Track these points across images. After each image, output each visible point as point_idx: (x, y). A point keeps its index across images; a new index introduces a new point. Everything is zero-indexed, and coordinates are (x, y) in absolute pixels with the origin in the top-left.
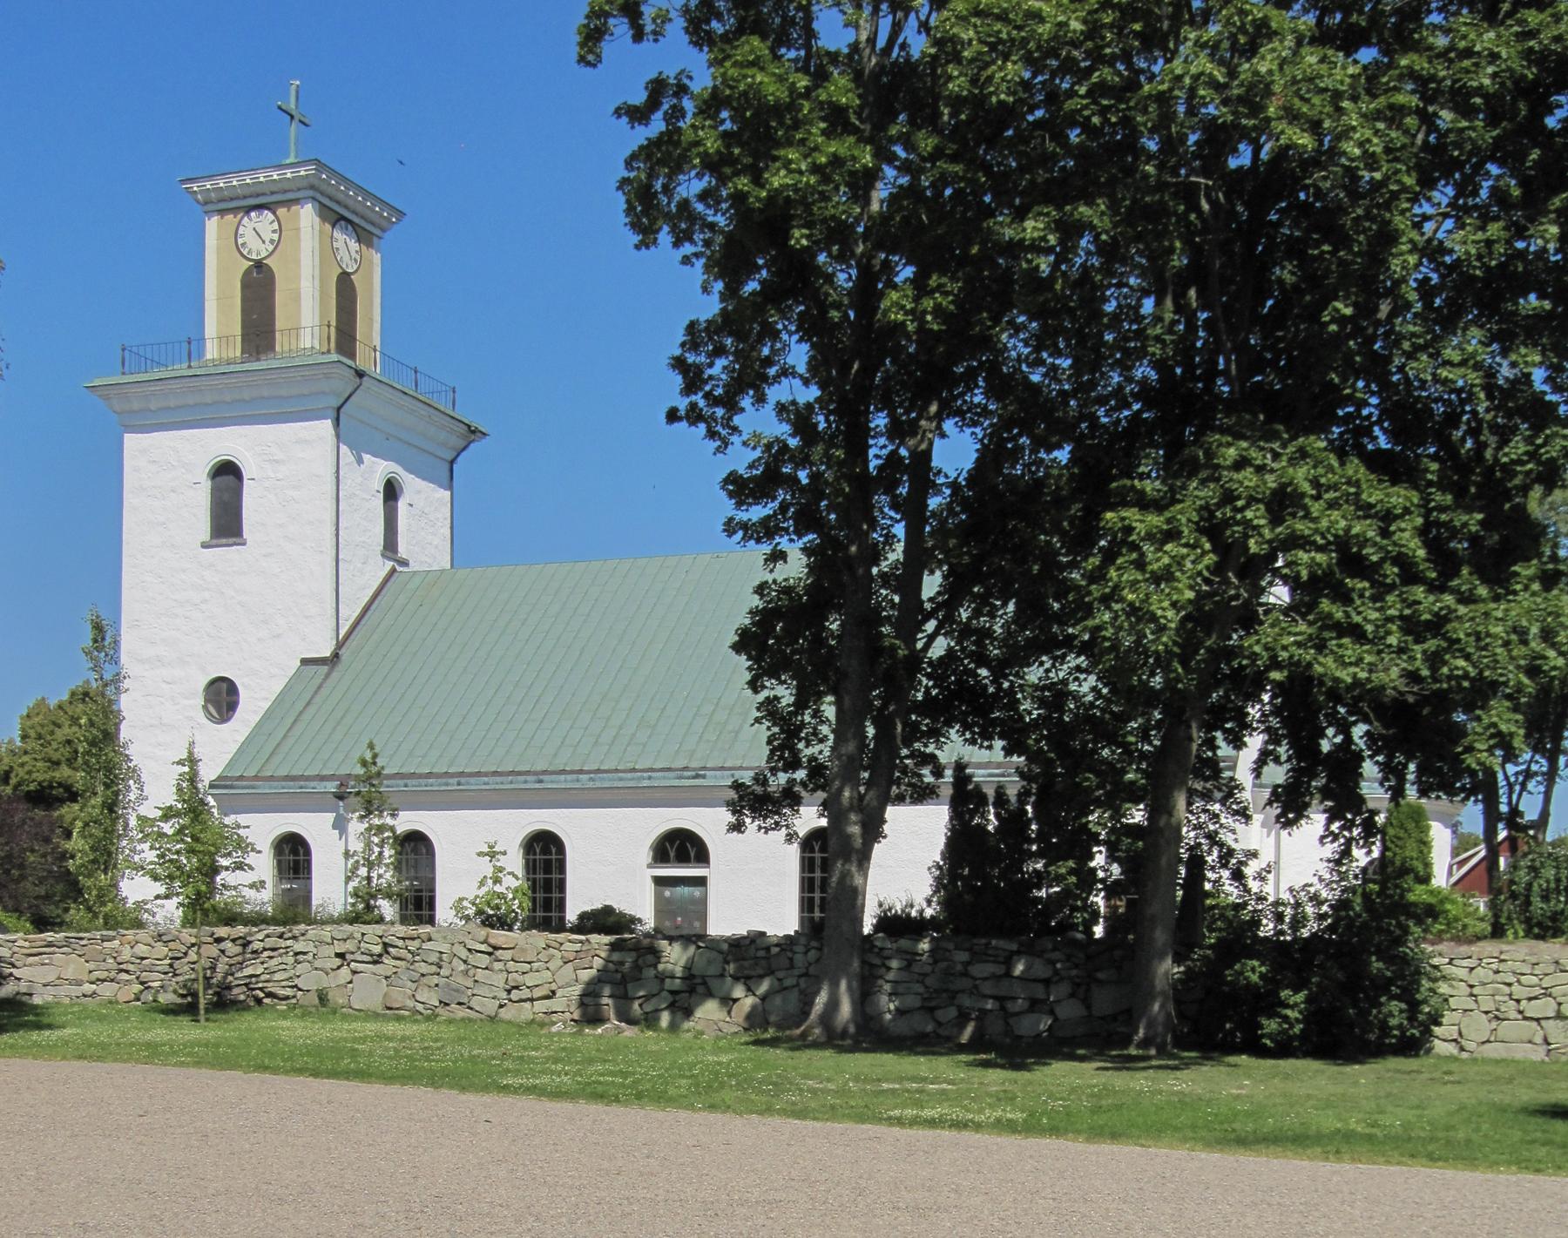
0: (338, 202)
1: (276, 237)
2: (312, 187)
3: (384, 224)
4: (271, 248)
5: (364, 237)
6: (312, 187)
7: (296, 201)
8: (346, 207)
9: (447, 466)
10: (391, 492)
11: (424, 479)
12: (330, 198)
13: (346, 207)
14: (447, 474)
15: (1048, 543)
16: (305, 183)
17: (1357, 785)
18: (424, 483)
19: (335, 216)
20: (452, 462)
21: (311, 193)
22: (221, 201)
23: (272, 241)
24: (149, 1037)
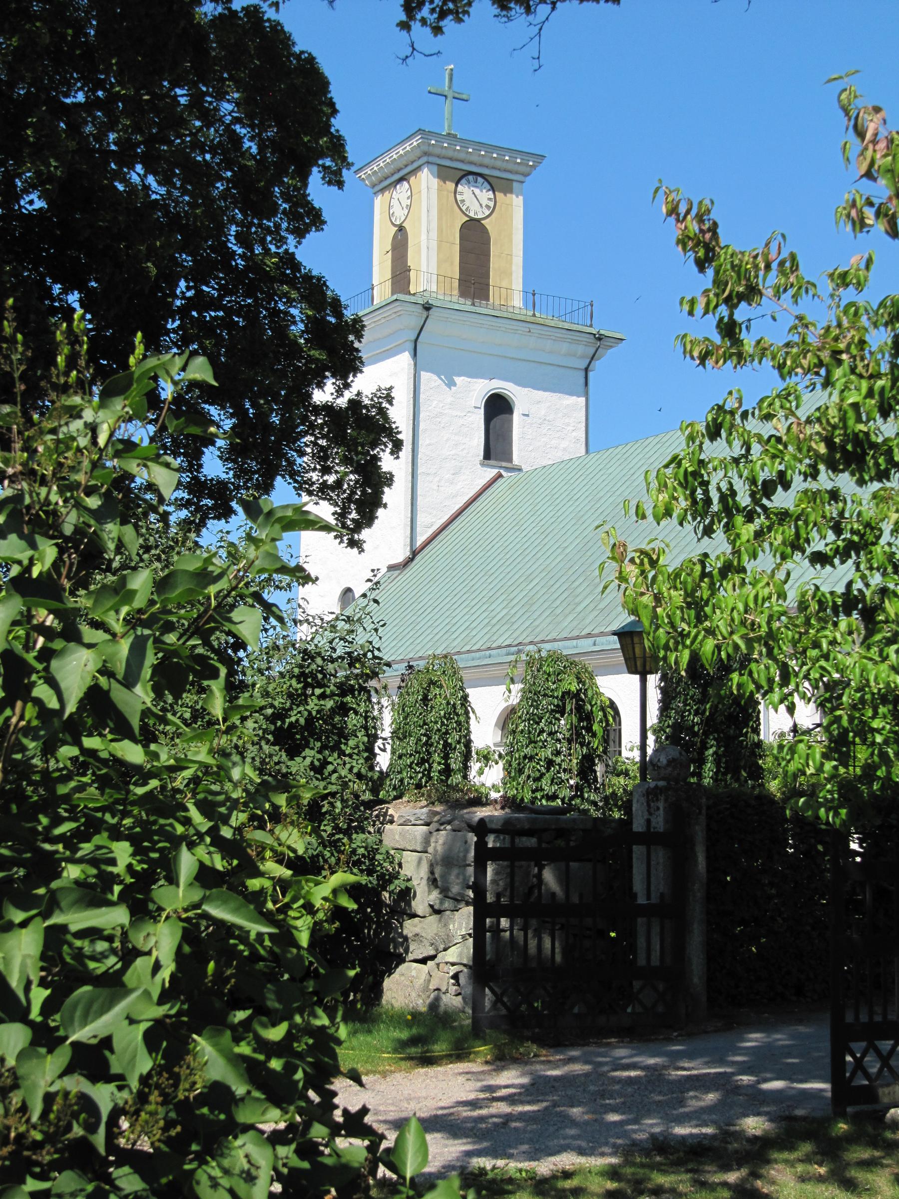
0: (462, 161)
1: (492, 204)
2: (426, 154)
3: (522, 169)
4: (487, 213)
5: (497, 184)
6: (426, 154)
7: (419, 168)
8: (471, 163)
9: (583, 373)
10: (498, 408)
11: (545, 390)
12: (451, 159)
13: (471, 163)
14: (583, 380)
15: (221, 334)
16: (418, 153)
17: (131, 1167)
18: (540, 393)
19: (457, 174)
20: (586, 370)
21: (425, 159)
22: (381, 181)
23: (488, 207)
24: (544, 1167)
